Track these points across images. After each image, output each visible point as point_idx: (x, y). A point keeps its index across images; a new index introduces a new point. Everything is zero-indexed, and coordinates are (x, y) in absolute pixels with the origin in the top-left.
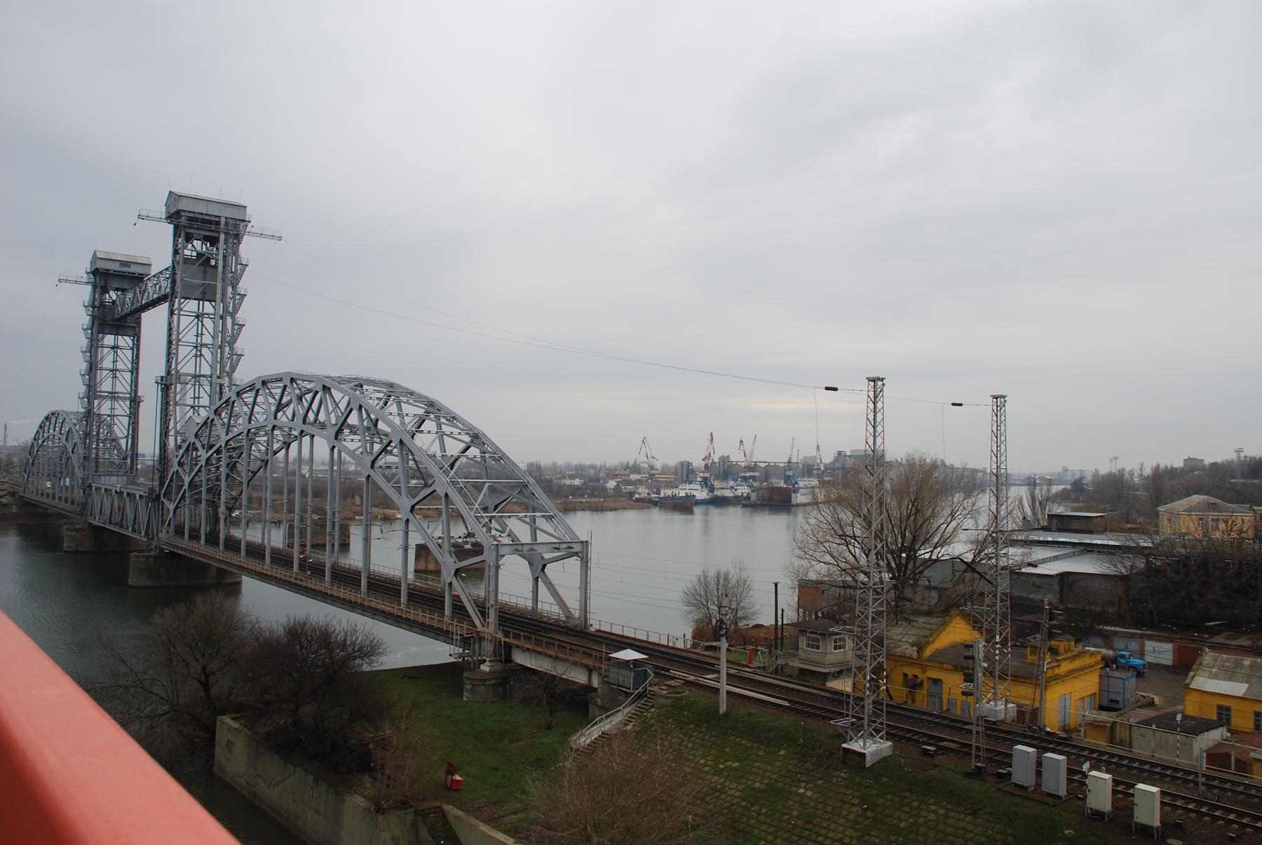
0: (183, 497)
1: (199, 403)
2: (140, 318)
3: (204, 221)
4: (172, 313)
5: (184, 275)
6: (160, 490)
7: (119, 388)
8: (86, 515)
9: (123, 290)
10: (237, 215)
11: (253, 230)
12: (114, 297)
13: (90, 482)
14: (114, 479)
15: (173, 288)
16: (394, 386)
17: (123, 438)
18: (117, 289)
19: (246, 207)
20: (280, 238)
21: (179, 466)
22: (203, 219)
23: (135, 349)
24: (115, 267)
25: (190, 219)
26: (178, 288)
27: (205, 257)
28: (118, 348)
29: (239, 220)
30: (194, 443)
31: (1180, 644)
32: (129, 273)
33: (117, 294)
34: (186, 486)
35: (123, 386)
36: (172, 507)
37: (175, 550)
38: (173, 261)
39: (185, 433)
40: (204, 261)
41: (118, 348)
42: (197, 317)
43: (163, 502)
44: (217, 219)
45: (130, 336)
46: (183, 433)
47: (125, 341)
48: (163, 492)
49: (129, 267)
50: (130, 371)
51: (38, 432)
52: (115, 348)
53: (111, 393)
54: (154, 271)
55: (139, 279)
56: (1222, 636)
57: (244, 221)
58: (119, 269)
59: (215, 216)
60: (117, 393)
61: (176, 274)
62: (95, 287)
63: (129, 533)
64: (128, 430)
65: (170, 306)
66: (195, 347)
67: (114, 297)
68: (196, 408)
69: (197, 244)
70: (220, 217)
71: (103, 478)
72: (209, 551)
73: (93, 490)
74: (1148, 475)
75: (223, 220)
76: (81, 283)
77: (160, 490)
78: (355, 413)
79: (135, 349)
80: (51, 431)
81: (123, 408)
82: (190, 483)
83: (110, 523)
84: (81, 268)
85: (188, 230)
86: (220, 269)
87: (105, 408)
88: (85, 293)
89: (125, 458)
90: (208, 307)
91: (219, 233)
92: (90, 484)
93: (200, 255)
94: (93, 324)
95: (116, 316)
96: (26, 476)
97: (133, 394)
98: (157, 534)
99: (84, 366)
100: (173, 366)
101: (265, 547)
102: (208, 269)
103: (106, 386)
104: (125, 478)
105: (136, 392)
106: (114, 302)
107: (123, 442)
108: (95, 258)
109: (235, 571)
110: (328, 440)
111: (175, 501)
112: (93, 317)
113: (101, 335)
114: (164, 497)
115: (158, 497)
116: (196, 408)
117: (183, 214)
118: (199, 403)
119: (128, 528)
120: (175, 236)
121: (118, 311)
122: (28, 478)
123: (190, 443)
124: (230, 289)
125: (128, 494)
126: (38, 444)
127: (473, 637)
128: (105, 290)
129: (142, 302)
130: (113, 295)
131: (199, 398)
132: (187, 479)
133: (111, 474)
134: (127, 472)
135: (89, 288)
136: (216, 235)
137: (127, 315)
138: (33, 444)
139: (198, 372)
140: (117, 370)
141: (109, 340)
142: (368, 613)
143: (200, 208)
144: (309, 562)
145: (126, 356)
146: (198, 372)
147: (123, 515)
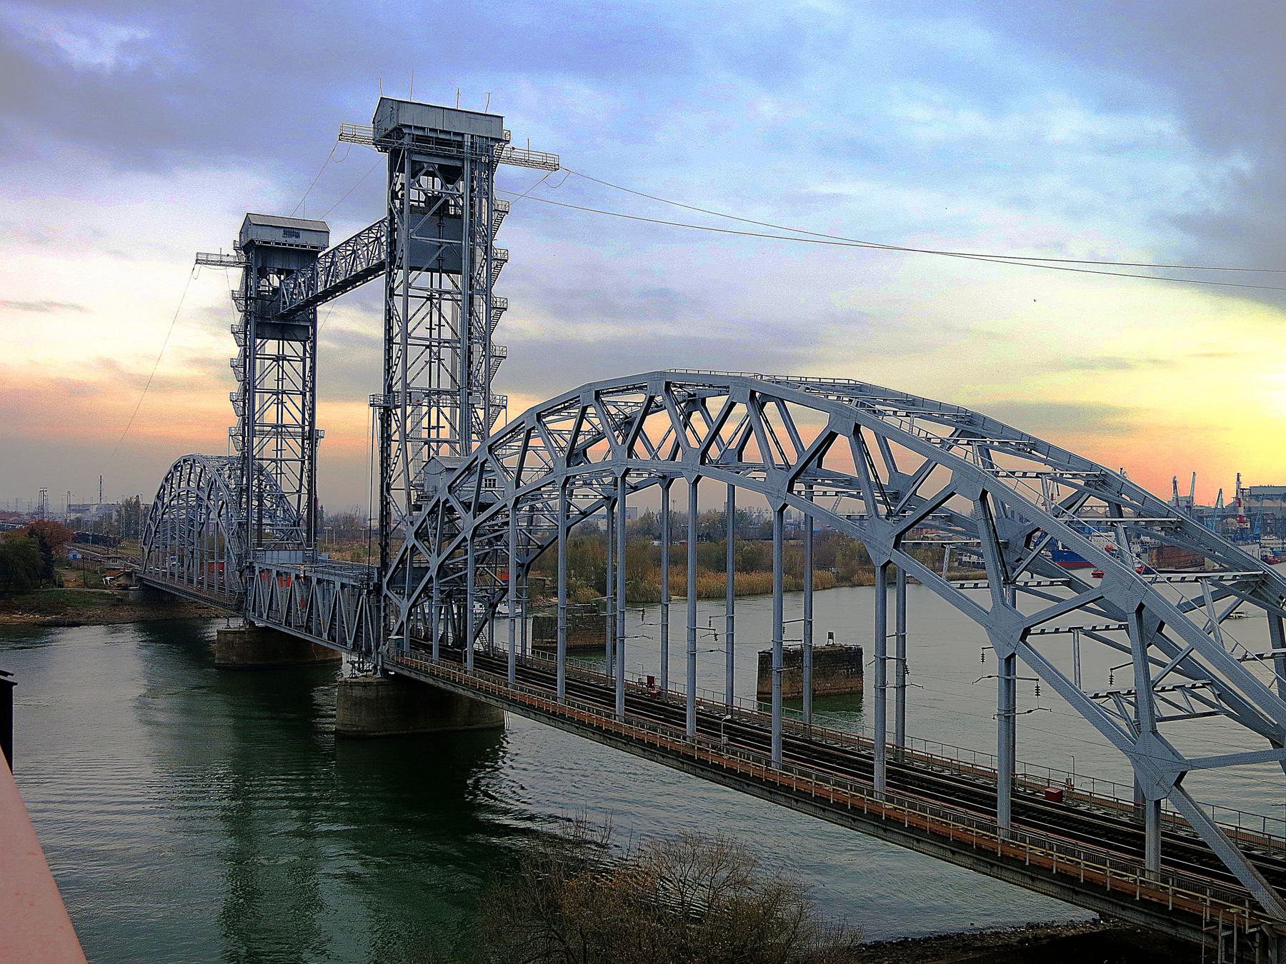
0: (426, 589)
1: (438, 436)
2: (315, 313)
3: (440, 142)
4: (391, 293)
5: (411, 230)
6: (380, 577)
7: (287, 419)
8: (246, 609)
9: (289, 273)
10: (482, 130)
11: (515, 155)
12: (276, 283)
13: (251, 560)
14: (284, 555)
15: (392, 254)
16: (862, 388)
17: (293, 493)
18: (279, 272)
19: (502, 117)
20: (556, 167)
21: (416, 538)
22: (437, 138)
23: (308, 360)
24: (277, 238)
25: (419, 139)
26: (403, 251)
27: (441, 202)
28: (284, 359)
29: (492, 139)
30: (447, 501)
31: (868, 659)
32: (297, 246)
33: (279, 278)
34: (433, 572)
35: (293, 413)
36: (405, 605)
37: (406, 673)
38: (391, 209)
39: (422, 485)
40: (438, 208)
41: (284, 359)
42: (430, 298)
43: (386, 595)
44: (459, 139)
45: (300, 341)
46: (419, 485)
47: (294, 348)
48: (385, 580)
49: (298, 236)
50: (301, 393)
51: (163, 487)
52: (279, 358)
53: (276, 426)
54: (334, 242)
55: (310, 255)
56: (384, 579)
57: (499, 140)
58: (283, 240)
59: (455, 134)
60: (284, 426)
61: (396, 230)
62: (248, 270)
63: (324, 641)
64: (301, 480)
65: (387, 283)
66: (427, 347)
67: (276, 283)
68: (434, 445)
69: (425, 181)
70: (462, 135)
71: (269, 553)
72: (449, 668)
73: (257, 572)
74: (648, 516)
75: (468, 139)
76: (228, 264)
77: (380, 577)
78: (842, 444)
79: (308, 360)
80: (183, 484)
81: (293, 447)
82: (441, 566)
83: (288, 623)
84: (226, 239)
85: (416, 158)
86: (466, 219)
87: (266, 448)
88: (234, 277)
89: (297, 524)
90: (447, 284)
91: (462, 160)
92: (251, 563)
93: (431, 200)
94: (247, 323)
95: (282, 311)
96: (146, 551)
97: (307, 428)
98: (377, 647)
99: (236, 387)
100: (398, 374)
101: (613, 683)
102: (446, 221)
103: (270, 416)
104: (300, 553)
105: (312, 424)
106: (276, 291)
107: (293, 500)
108: (248, 224)
109: (493, 702)
110: (766, 493)
111: (410, 597)
112: (247, 314)
113: (258, 341)
114: (388, 589)
115: (378, 588)
116: (434, 445)
117: (405, 131)
118: (438, 436)
119: (320, 634)
120: (392, 170)
121: (285, 303)
122: (149, 552)
123: (439, 501)
124: (479, 253)
125: (319, 582)
126: (163, 504)
127: (1261, 932)
128: (263, 273)
129: (307, 295)
130: (275, 281)
131: (281, 450)
132: (434, 562)
133: (278, 548)
134: (301, 544)
135: (239, 272)
136: (458, 164)
137: (300, 308)
138: (156, 504)
139: (434, 386)
140: (284, 392)
141: (271, 347)
142: (895, 836)
143: (429, 122)
144: (726, 720)
145: (294, 370)
146: (434, 386)
147: (310, 613)
